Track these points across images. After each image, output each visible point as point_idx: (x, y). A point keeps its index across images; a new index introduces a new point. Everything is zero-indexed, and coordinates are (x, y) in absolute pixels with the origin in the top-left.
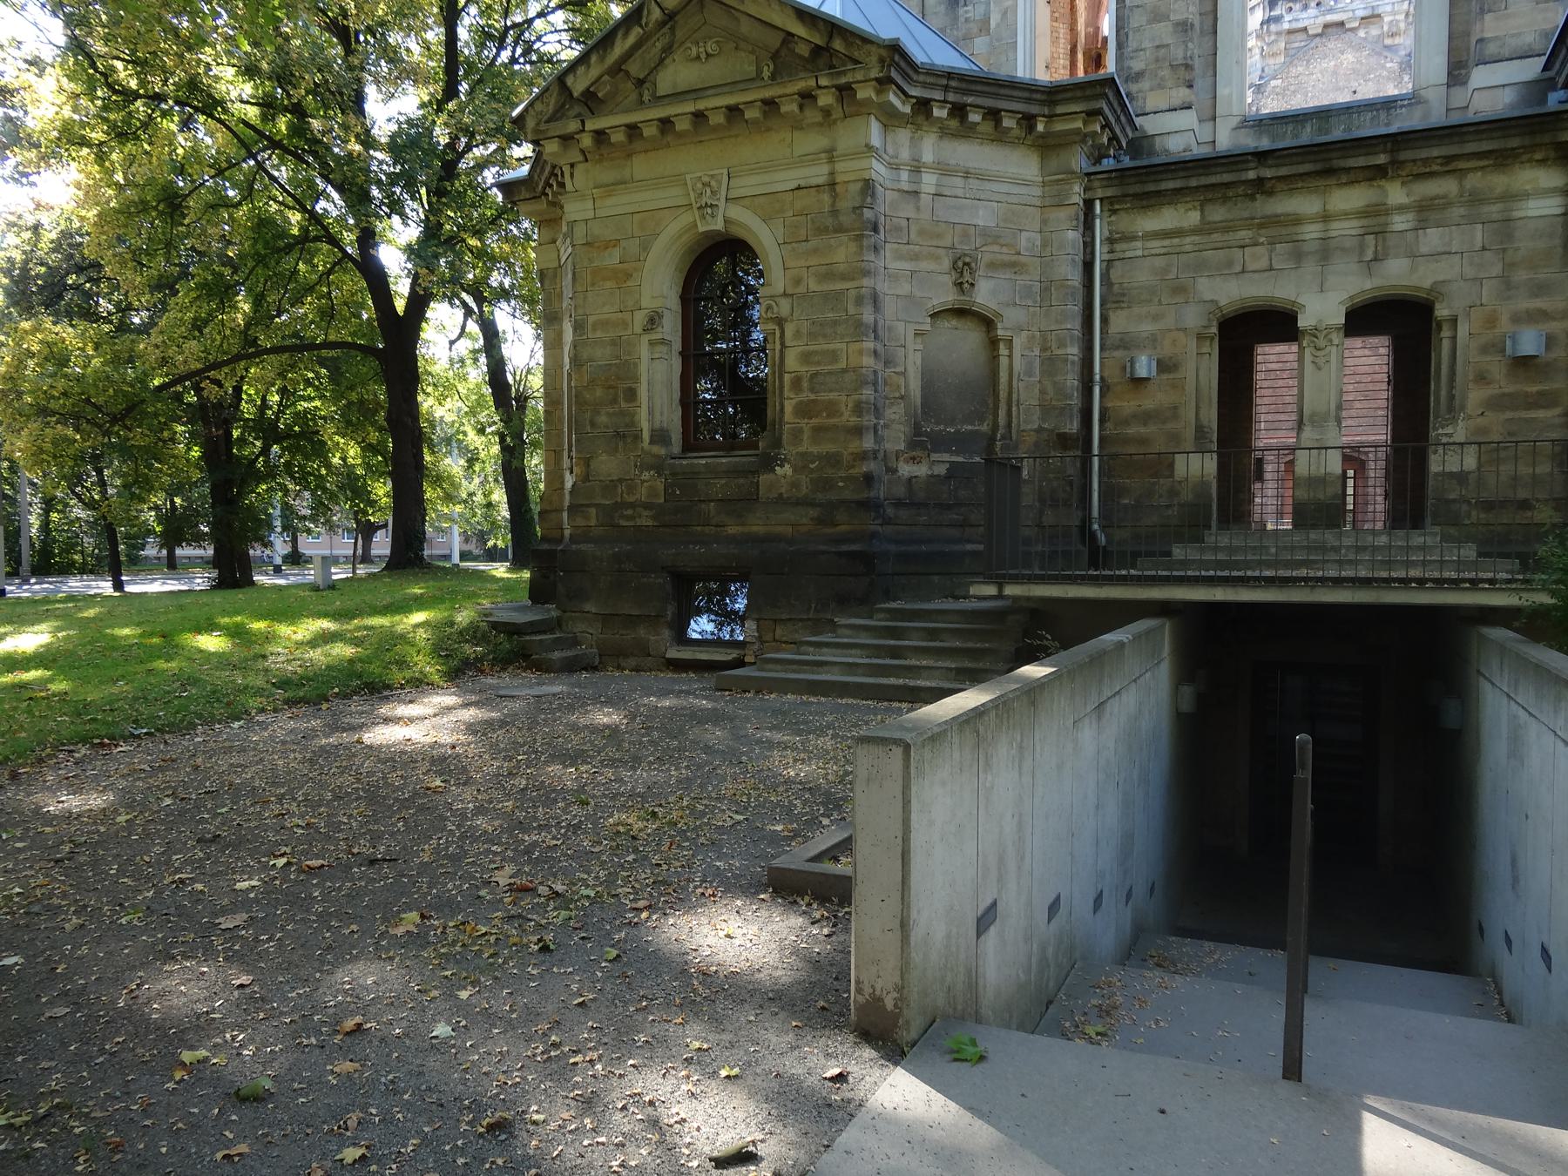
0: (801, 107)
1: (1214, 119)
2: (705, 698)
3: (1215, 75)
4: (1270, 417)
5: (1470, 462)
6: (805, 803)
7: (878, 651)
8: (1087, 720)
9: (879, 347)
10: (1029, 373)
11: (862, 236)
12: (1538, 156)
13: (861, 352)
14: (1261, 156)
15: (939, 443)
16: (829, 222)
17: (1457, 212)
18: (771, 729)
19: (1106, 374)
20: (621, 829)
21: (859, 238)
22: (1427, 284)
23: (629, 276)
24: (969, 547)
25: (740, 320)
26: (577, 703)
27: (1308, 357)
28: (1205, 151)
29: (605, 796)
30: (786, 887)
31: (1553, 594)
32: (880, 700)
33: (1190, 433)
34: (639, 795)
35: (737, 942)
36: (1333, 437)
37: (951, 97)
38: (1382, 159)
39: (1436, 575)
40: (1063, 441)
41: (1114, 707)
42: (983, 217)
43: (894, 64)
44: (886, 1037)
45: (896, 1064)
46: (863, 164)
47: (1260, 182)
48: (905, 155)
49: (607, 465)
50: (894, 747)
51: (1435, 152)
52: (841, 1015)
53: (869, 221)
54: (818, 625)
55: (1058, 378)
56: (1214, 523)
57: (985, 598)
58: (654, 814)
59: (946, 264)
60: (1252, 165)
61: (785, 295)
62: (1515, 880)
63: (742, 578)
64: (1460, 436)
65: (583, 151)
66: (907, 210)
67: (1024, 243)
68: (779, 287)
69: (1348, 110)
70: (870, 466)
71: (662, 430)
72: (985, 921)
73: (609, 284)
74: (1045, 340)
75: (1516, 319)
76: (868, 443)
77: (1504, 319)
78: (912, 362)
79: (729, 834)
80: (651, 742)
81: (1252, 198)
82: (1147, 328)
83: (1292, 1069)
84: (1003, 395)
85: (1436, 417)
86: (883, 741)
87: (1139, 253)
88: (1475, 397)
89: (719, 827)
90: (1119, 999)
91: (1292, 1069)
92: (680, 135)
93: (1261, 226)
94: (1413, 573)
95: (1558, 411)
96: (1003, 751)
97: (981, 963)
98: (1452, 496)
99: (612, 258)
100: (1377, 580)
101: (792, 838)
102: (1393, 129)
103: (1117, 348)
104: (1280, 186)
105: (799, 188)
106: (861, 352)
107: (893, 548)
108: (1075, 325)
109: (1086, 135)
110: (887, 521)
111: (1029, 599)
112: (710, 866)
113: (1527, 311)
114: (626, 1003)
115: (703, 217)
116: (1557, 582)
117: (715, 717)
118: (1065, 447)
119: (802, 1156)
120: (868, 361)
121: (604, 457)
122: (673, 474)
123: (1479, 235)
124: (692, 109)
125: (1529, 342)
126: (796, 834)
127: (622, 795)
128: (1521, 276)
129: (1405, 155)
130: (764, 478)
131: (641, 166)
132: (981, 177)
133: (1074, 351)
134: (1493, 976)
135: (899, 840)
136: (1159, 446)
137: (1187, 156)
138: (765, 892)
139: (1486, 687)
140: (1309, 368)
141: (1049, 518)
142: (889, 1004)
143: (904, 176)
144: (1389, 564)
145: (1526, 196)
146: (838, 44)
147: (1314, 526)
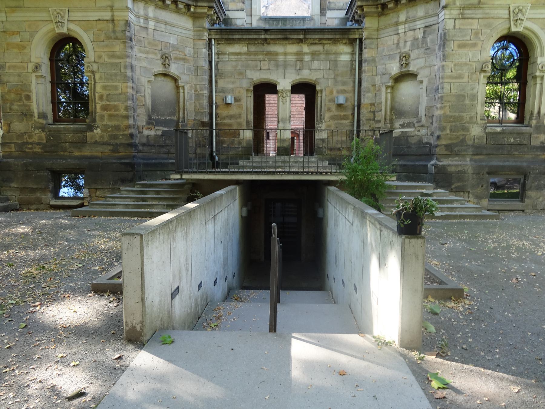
2: (67, 220)
4: (271, 119)
5: (326, 136)
6: (108, 257)
7: (137, 199)
8: (210, 221)
9: (134, 86)
10: (190, 98)
11: (126, 42)
13: (127, 87)
14: (266, 31)
15: (158, 123)
17: (322, 57)
18: (95, 230)
19: (217, 101)
20: (28, 274)
21: (125, 43)
22: (314, 79)
23: (24, 48)
24: (171, 161)
25: (76, 71)
26: (10, 225)
27: (280, 100)
28: (247, 26)
29: (21, 262)
30: (99, 290)
31: (346, 176)
32: (138, 217)
33: (245, 123)
34: (37, 260)
35: (78, 313)
38: (301, 37)
40: (203, 124)
41: (220, 216)
42: (173, 40)
44: (136, 339)
45: (141, 349)
46: (125, 14)
47: (265, 39)
48: (142, 12)
49: (19, 126)
50: (136, 236)
51: (316, 37)
52: (120, 335)
53: (128, 37)
54: (113, 190)
55: (201, 102)
56: (253, 154)
57: (175, 179)
58: (43, 267)
59: (159, 56)
61: (95, 62)
62: (336, 262)
63: (82, 173)
64: (323, 128)
66: (143, 34)
67: (187, 51)
68: (92, 59)
69: (292, 19)
70: (132, 131)
71: (43, 113)
72: (175, 293)
73: (15, 50)
74: (196, 88)
75: (338, 92)
76: (131, 122)
77: (335, 92)
78: (147, 92)
79: (76, 272)
80: (43, 239)
81: (263, 44)
82: (230, 86)
83: (273, 328)
84: (181, 106)
86: (133, 234)
87: (227, 59)
88: (327, 115)
89: (71, 270)
90: (222, 313)
91: (273, 328)
92: (391, 9)
93: (266, 55)
94: (311, 170)
95: (349, 121)
96: (180, 234)
97: (173, 308)
98: (321, 146)
99: (17, 39)
100: (300, 172)
101: (103, 271)
102: (305, 28)
103: (221, 92)
104: (272, 42)
105: (99, 20)
106: (127, 87)
107: (142, 161)
108: (206, 83)
109: (208, 15)
110: (139, 151)
111: (192, 180)
112: (67, 285)
114: (29, 344)
115: (58, 27)
116: (348, 173)
117: (71, 227)
118: (204, 126)
119: (104, 389)
120: (130, 91)
121: (17, 123)
122: (50, 131)
125: (341, 100)
126: (104, 270)
127: (29, 261)
128: (339, 79)
130: (89, 134)
132: (172, 25)
133: (206, 92)
134: (331, 290)
135: (140, 270)
136: (235, 127)
137: (243, 27)
138: (91, 293)
139: (329, 204)
140: (281, 103)
141: (199, 151)
142: (138, 328)
143: (142, 21)
144: (303, 167)
145: (341, 54)
147: (283, 155)
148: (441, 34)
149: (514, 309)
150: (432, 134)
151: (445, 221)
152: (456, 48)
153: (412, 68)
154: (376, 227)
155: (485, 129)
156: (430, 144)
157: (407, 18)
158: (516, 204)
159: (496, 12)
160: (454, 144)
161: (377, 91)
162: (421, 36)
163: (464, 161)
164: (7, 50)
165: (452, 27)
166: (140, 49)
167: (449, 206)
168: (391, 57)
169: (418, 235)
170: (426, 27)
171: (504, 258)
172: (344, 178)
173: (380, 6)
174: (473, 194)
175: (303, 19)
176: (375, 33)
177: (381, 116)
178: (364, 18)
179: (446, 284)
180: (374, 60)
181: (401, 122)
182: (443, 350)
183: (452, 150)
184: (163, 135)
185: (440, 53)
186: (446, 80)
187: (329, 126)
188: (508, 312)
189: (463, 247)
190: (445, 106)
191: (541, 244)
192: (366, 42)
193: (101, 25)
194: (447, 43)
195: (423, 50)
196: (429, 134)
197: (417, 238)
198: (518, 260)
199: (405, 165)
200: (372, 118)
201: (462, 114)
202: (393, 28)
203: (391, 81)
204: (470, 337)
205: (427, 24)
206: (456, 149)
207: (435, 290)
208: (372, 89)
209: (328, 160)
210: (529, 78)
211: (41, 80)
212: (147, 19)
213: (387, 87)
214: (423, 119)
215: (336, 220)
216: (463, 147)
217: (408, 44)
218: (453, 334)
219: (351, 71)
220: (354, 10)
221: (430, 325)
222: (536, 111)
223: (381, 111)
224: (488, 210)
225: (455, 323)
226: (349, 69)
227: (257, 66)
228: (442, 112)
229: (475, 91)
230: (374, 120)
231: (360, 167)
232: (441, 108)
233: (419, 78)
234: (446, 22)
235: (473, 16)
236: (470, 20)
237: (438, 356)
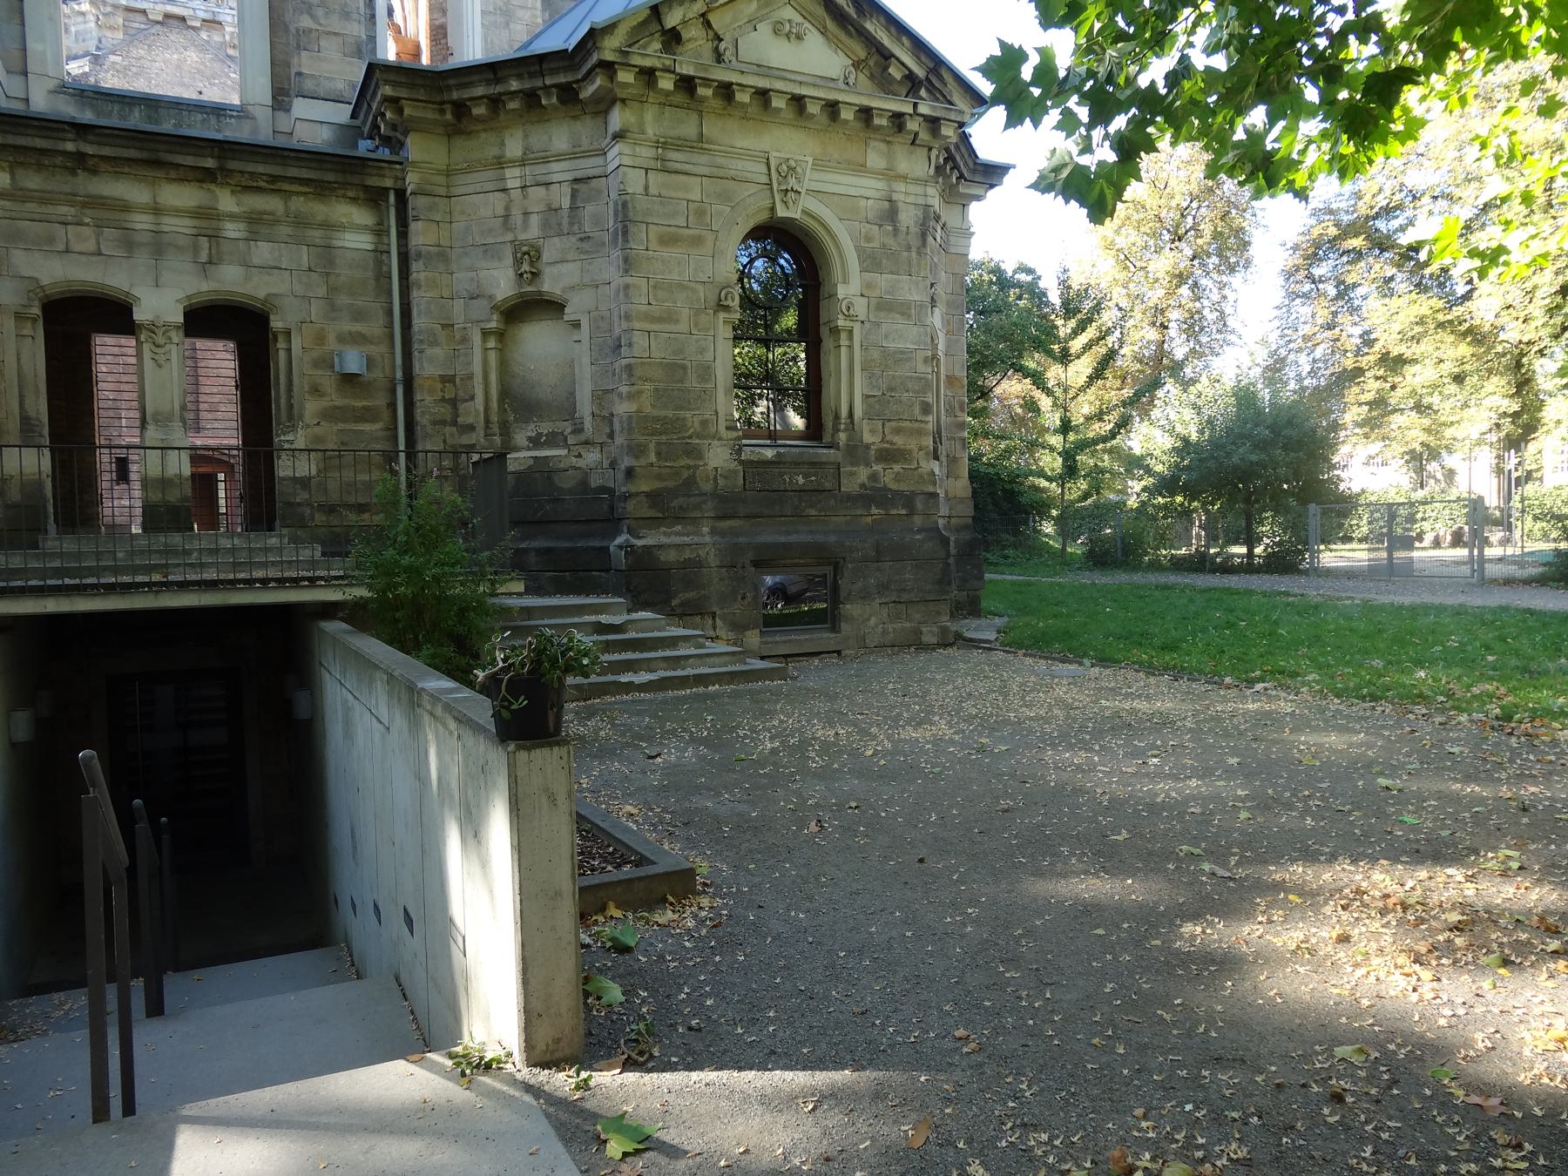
1: (25, 74)
3: (23, 25)
12: (350, 194)
14: (81, 130)
17: (284, 230)
22: (261, 294)
27: (147, 355)
31: (370, 588)
33: (13, 425)
36: (179, 437)
38: (210, 163)
39: (279, 575)
47: (80, 157)
51: (261, 169)
56: (52, 527)
60: (70, 136)
62: (355, 848)
64: (300, 444)
69: (178, 105)
75: (341, 339)
77: (331, 338)
85: (278, 424)
88: (311, 407)
92: (478, 119)
93: (84, 205)
94: (259, 574)
102: (219, 137)
104: (103, 166)
113: (350, 333)
123: (305, 258)
125: (353, 362)
128: (343, 300)
129: (232, 165)
140: (148, 364)
144: (236, 566)
145: (342, 227)
148: (616, 204)
149: (810, 899)
150: (613, 465)
151: (660, 695)
152: (653, 245)
153: (550, 285)
154: (445, 725)
155: (739, 452)
156: (610, 491)
157: (527, 150)
158: (822, 638)
159: (740, 165)
161: (459, 343)
163: (695, 534)
165: (640, 190)
167: (668, 653)
169: (552, 736)
171: (792, 774)
172: (362, 592)
173: (448, 107)
174: (723, 619)
175: (218, 111)
176: (441, 180)
177: (474, 411)
178: (406, 133)
179: (654, 863)
180: (442, 256)
181: (531, 430)
182: (642, 1047)
183: (668, 506)
185: (616, 254)
186: (637, 325)
187: (318, 439)
188: (798, 910)
189: (703, 758)
190: (640, 392)
191: (874, 730)
192: (416, 203)
194: (632, 229)
195: (574, 239)
196: (606, 464)
197: (550, 745)
198: (823, 775)
199: (549, 550)
200: (448, 418)
202: (490, 174)
203: (495, 317)
204: (709, 995)
205: (579, 174)
206: (675, 503)
207: (600, 890)
208: (442, 335)
209: (323, 544)
213: (486, 334)
214: (588, 424)
215: (348, 722)
216: (692, 500)
217: (534, 220)
218: (668, 997)
219: (377, 280)
221: (611, 984)
222: (844, 412)
223: (472, 398)
224: (762, 658)
225: (672, 965)
226: (370, 274)
227: (51, 240)
228: (634, 407)
229: (709, 356)
230: (454, 423)
231: (406, 560)
232: (631, 397)
233: (570, 313)
234: (625, 174)
235: (687, 167)
236: (682, 178)
237: (629, 1065)
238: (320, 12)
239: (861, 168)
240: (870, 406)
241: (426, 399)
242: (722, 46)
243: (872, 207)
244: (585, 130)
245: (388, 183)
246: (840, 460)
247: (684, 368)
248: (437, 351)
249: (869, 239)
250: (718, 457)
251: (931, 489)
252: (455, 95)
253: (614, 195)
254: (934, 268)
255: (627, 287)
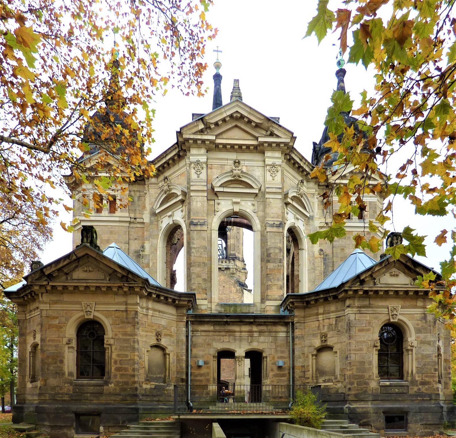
0: (118, 290)
16: (125, 320)
22: (261, 348)
23: (61, 327)
33: (212, 379)
37: (157, 293)
38: (252, 320)
40: (182, 380)
42: (163, 322)
43: (145, 284)
46: (136, 307)
47: (227, 322)
49: (53, 382)
56: (328, 407)
59: (154, 334)
61: (112, 338)
65: (47, 290)
66: (145, 319)
73: (54, 329)
78: (146, 358)
82: (201, 353)
84: (167, 368)
88: (271, 374)
95: (286, 378)
99: (56, 322)
105: (117, 310)
118: (183, 382)
121: (52, 379)
124: (85, 285)
125: (281, 364)
129: (257, 320)
131: (66, 298)
133: (184, 358)
145: (279, 332)
146: (130, 276)
153: (329, 343)
156: (344, 394)
157: (324, 310)
159: (380, 310)
160: (359, 393)
162: (334, 323)
164: (49, 328)
166: (142, 330)
168: (314, 335)
170: (337, 317)
176: (303, 319)
177: (309, 374)
181: (323, 378)
184: (155, 389)
185: (347, 335)
186: (352, 352)
190: (353, 369)
193: (117, 314)
194: (351, 328)
195: (336, 331)
196: (343, 387)
201: (364, 374)
205: (338, 316)
208: (302, 356)
210: (404, 350)
211: (71, 350)
212: (148, 309)
213: (313, 355)
214: (339, 377)
217: (326, 327)
219: (287, 343)
220: (287, 303)
222: (410, 372)
227: (220, 340)
229: (371, 359)
230: (304, 377)
232: (350, 370)
233: (334, 350)
238: (273, 280)
239: (416, 307)
240: (418, 370)
241: (298, 373)
242: (376, 281)
243: (418, 316)
244: (339, 305)
245: (290, 321)
246: (408, 384)
247: (364, 362)
248: (301, 360)
249: (418, 325)
250: (373, 384)
251: (437, 392)
252: (307, 299)
253: (347, 320)
254: (439, 329)
255: (350, 343)
